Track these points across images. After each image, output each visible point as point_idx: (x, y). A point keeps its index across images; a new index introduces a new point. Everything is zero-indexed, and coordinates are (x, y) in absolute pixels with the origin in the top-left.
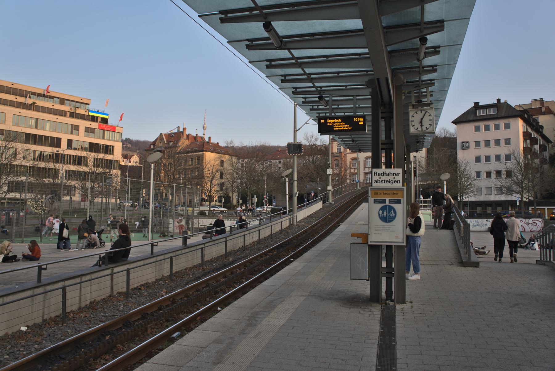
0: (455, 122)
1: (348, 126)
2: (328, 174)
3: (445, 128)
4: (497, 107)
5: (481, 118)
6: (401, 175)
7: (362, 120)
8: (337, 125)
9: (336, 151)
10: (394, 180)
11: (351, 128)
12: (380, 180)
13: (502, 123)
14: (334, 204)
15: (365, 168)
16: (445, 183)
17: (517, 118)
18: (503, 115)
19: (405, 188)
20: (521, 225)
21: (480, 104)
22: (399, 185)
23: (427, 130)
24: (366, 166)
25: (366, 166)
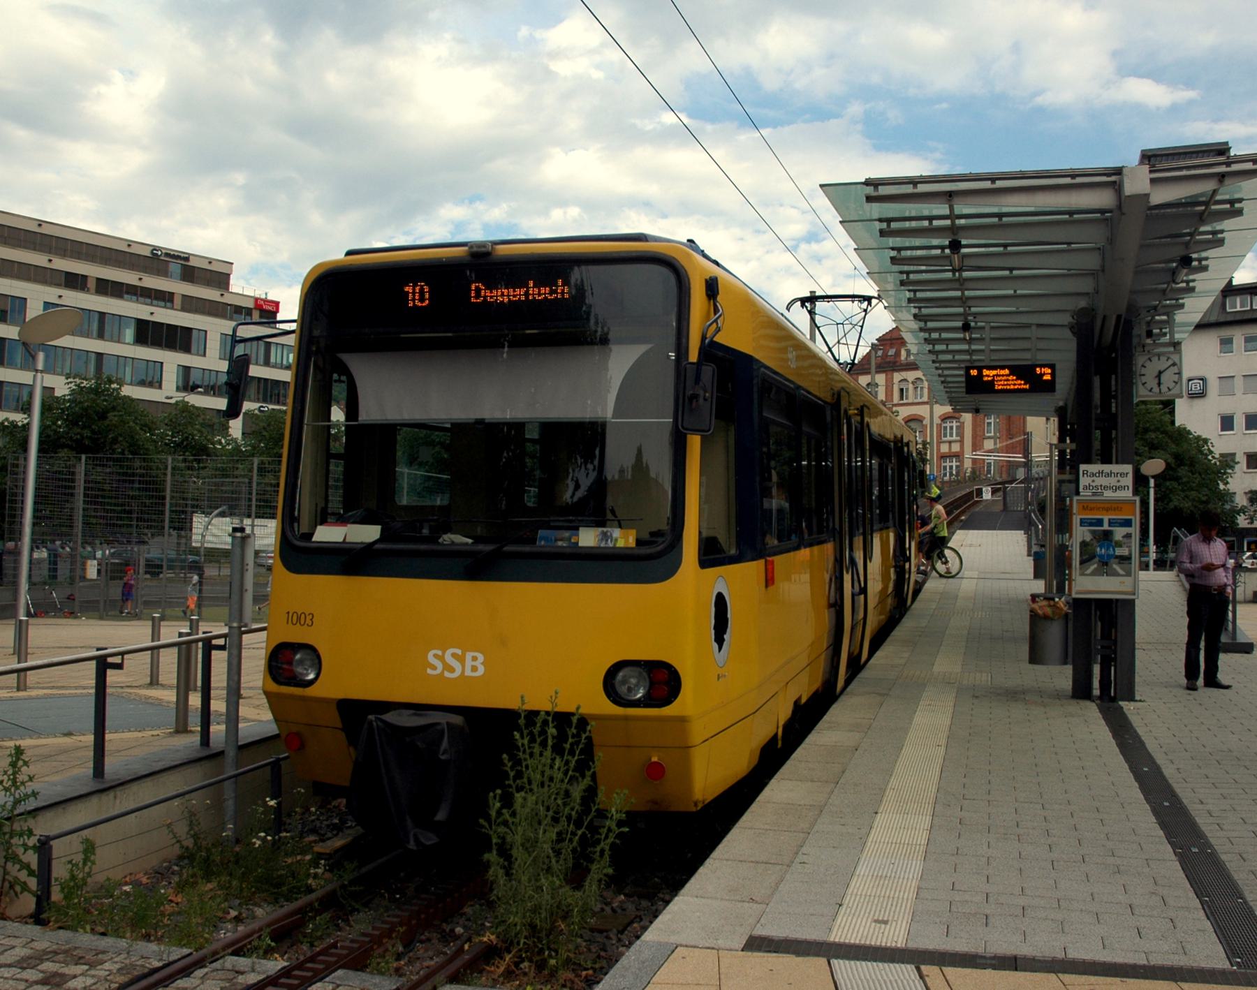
5: (1238, 318)
6: (1130, 476)
7: (1049, 371)
8: (1001, 380)
10: (1118, 484)
12: (1094, 484)
16: (1152, 482)
19: (1137, 499)
22: (1128, 494)
23: (1171, 392)
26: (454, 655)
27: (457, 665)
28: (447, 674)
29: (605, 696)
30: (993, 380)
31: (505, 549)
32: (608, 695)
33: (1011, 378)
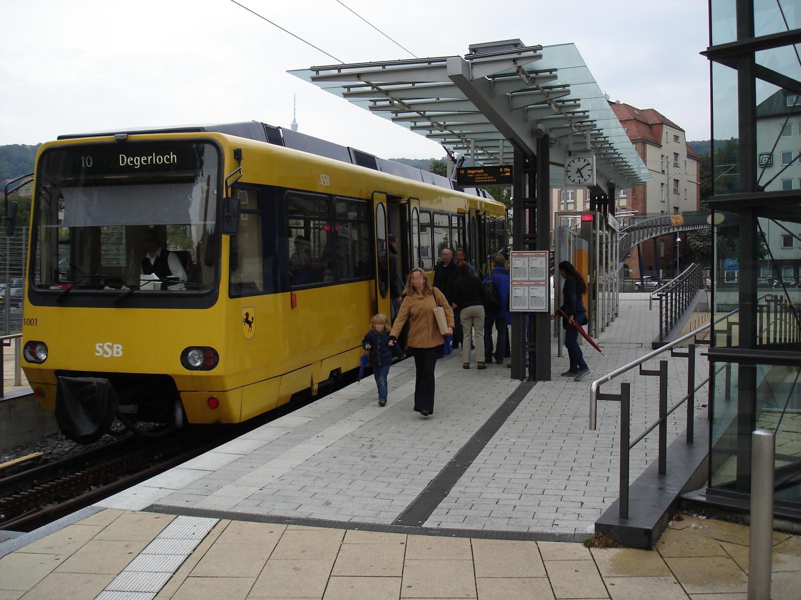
1: (492, 178)
7: (509, 170)
26: (108, 346)
27: (109, 351)
28: (105, 356)
29: (181, 365)
30: (474, 177)
31: (135, 292)
32: (183, 364)
33: (485, 175)
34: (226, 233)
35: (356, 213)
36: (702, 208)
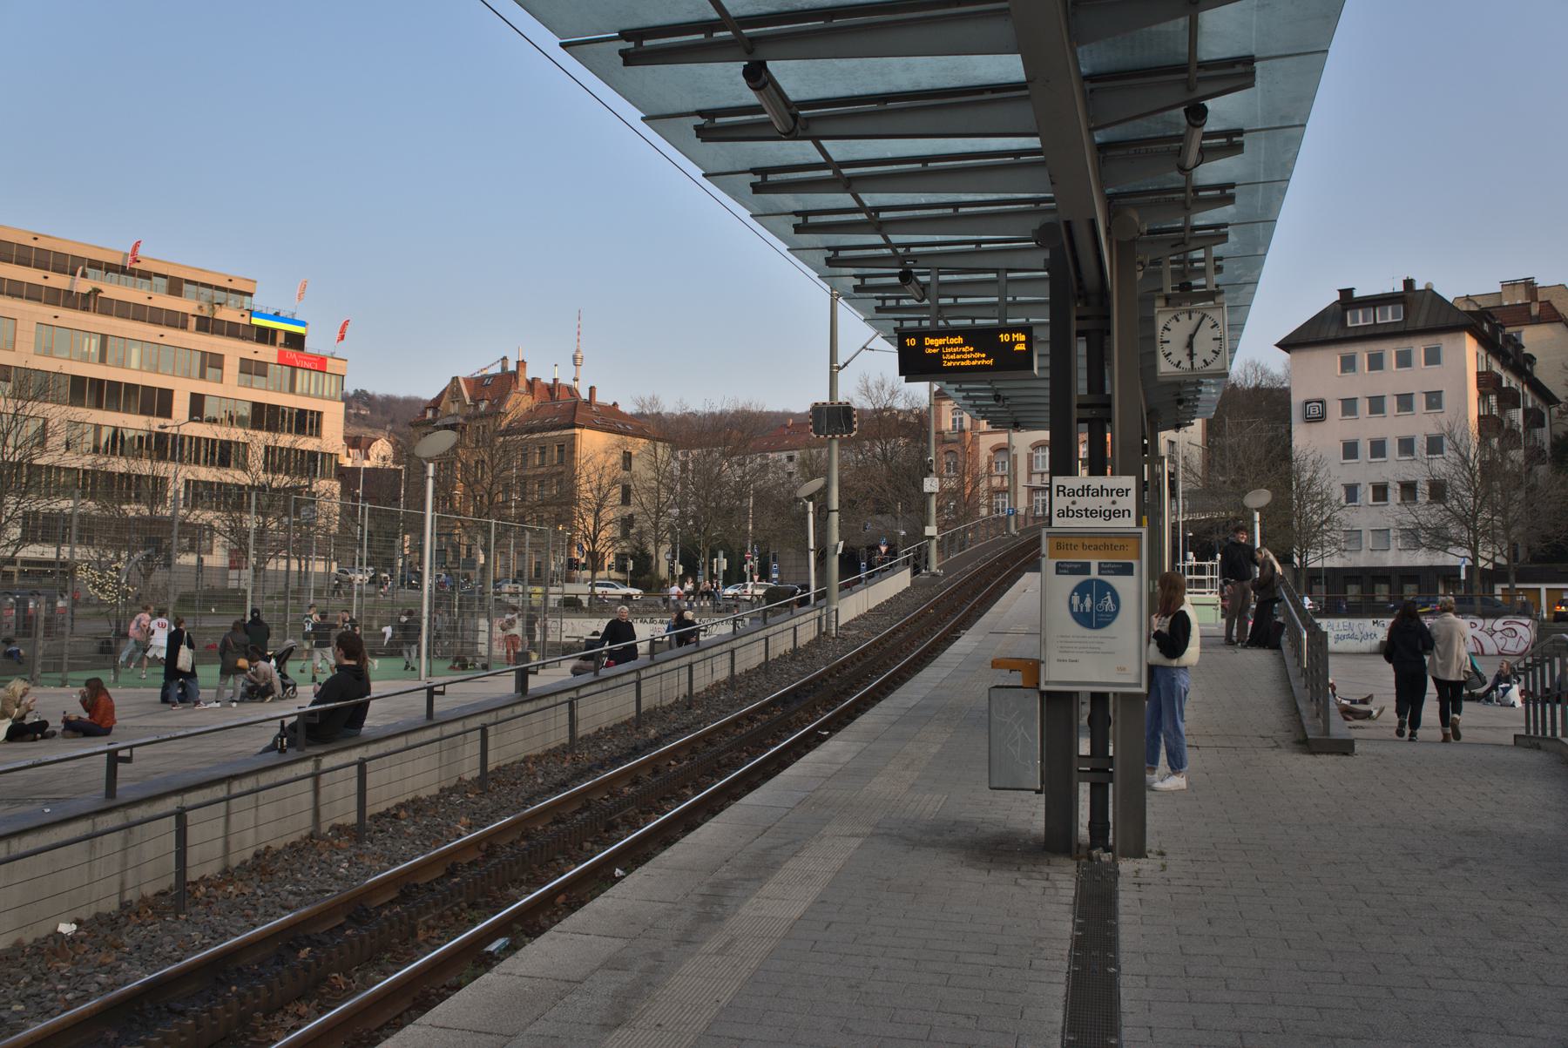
0: (1286, 345)
1: (984, 355)
2: (925, 490)
3: (1257, 362)
4: (1404, 303)
5: (1360, 333)
6: (1132, 493)
7: (1023, 338)
8: (951, 353)
9: (950, 427)
10: (1113, 508)
11: (991, 362)
12: (1075, 508)
13: (1418, 347)
14: (945, 575)
15: (1030, 473)
17: (1462, 334)
18: (1420, 325)
19: (1144, 531)
20: (1473, 637)
21: (1356, 294)
22: (1129, 523)
23: (1207, 368)
24: (1035, 470)
25: (1035, 470)
34: (236, 662)
35: (1048, 432)
36: (215, 487)
